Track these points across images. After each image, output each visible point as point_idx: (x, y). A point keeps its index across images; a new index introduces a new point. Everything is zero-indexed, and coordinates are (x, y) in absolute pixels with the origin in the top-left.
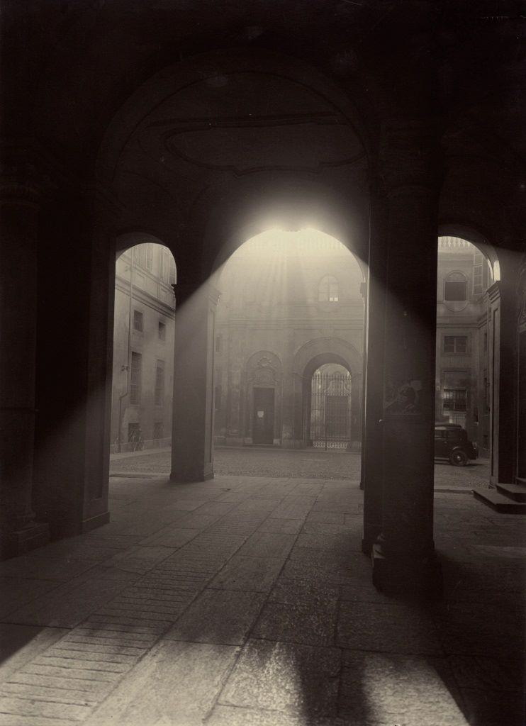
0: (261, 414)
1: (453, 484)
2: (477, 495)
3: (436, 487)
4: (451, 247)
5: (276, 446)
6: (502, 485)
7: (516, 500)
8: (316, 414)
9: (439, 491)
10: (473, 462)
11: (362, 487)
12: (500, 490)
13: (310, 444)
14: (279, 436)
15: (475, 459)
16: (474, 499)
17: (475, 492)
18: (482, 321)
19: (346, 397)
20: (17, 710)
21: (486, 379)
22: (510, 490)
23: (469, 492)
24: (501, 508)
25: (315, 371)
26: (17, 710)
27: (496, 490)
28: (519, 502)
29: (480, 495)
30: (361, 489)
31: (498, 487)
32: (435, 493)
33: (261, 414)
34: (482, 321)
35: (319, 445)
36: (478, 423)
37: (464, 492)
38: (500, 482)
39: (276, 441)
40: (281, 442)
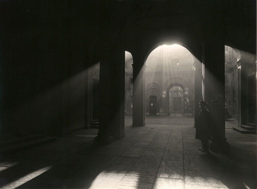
0: (152, 105)
1: (230, 127)
2: (234, 129)
3: (226, 127)
5: (158, 116)
6: (241, 125)
7: (248, 130)
8: (170, 104)
9: (227, 128)
12: (242, 127)
13: (169, 115)
14: (159, 112)
15: (230, 118)
16: (233, 130)
18: (232, 69)
19: (180, 98)
20: (183, 186)
21: (233, 90)
22: (246, 127)
23: (231, 128)
24: (242, 132)
25: (170, 89)
26: (183, 186)
28: (249, 130)
30: (195, 128)
31: (241, 126)
33: (152, 105)
34: (232, 69)
35: (171, 115)
36: (230, 106)
37: (230, 128)
38: (242, 125)
39: (157, 114)
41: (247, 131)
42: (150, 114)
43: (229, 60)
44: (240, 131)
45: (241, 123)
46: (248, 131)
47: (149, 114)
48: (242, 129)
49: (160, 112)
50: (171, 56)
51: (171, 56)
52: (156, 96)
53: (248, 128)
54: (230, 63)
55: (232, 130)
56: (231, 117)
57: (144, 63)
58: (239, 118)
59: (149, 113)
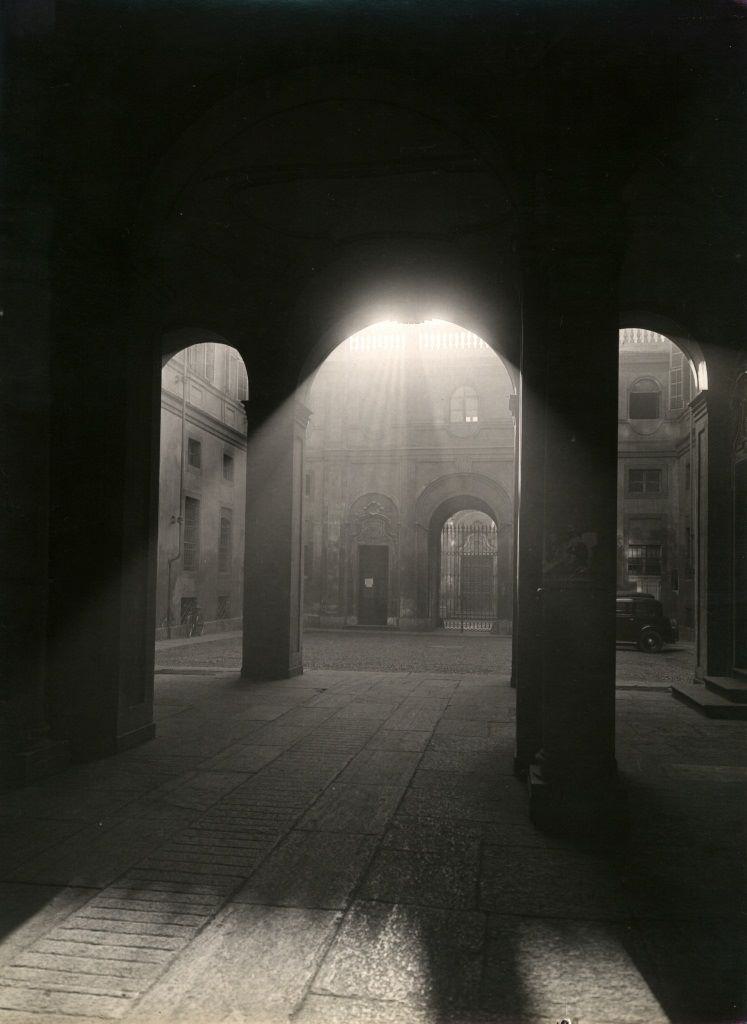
0: (369, 583)
1: (643, 679)
2: (677, 694)
3: (618, 683)
4: (638, 344)
6: (713, 680)
10: (672, 646)
11: (513, 684)
12: (711, 687)
13: (440, 624)
14: (395, 613)
15: (674, 642)
17: (674, 689)
19: (490, 558)
21: (688, 529)
24: (710, 712)
27: (704, 686)
29: (688, 698)
31: (705, 680)
32: (617, 692)
33: (369, 583)
35: (451, 626)
36: (677, 592)
38: (709, 675)
39: (390, 620)
40: (398, 621)
41: (732, 704)
42: (359, 623)
43: (673, 406)
44: (724, 690)
45: (705, 668)
46: (731, 707)
47: (357, 621)
48: (710, 694)
49: (401, 615)
50: (414, 359)
51: (414, 359)
52: (385, 549)
53: (731, 692)
54: (678, 418)
55: (668, 697)
56: (678, 638)
57: (302, 381)
58: (300, 578)
59: (354, 618)
